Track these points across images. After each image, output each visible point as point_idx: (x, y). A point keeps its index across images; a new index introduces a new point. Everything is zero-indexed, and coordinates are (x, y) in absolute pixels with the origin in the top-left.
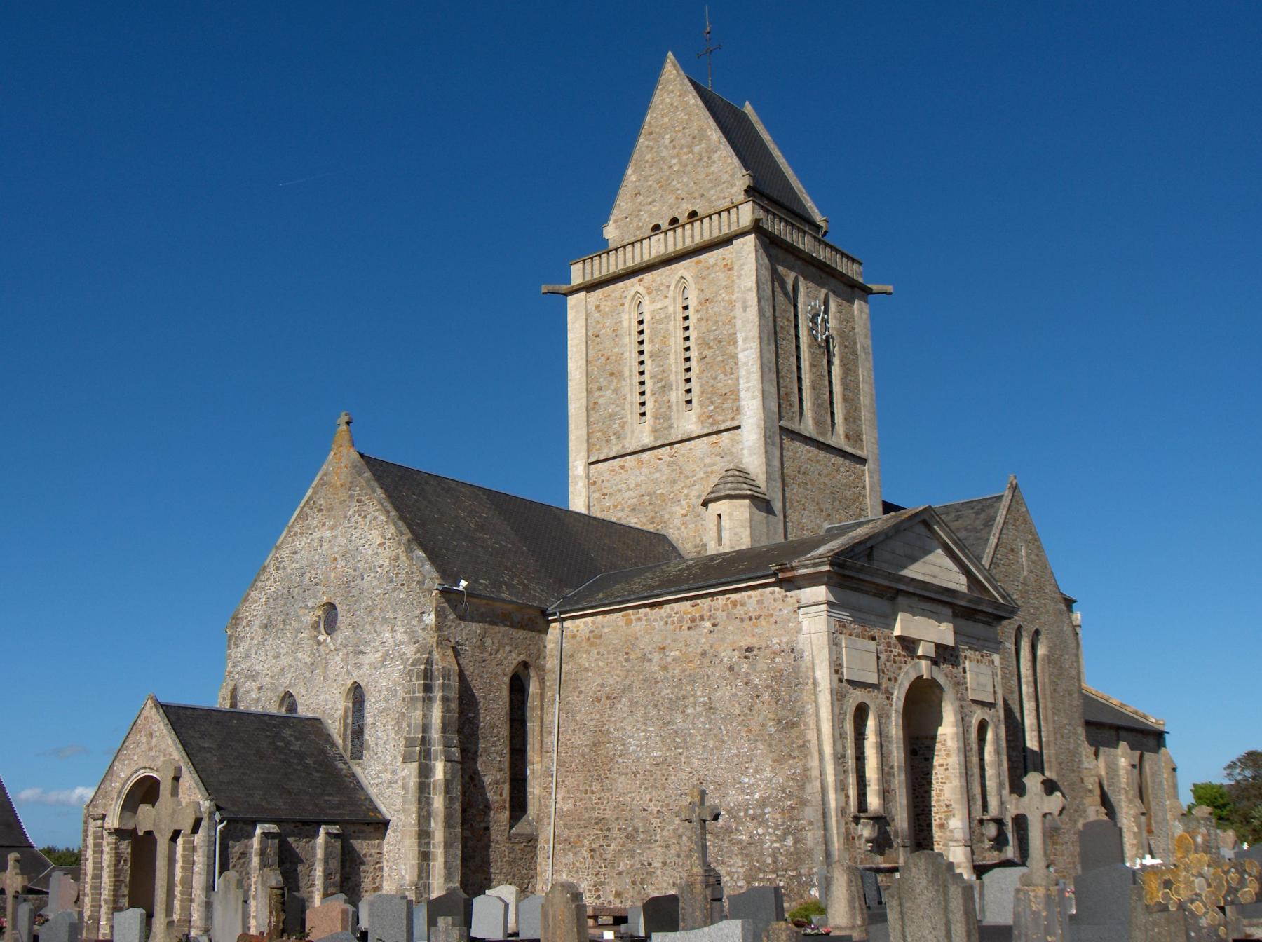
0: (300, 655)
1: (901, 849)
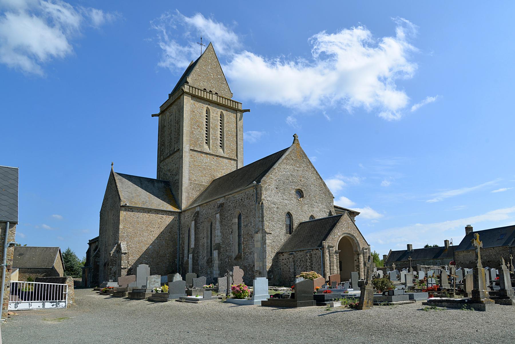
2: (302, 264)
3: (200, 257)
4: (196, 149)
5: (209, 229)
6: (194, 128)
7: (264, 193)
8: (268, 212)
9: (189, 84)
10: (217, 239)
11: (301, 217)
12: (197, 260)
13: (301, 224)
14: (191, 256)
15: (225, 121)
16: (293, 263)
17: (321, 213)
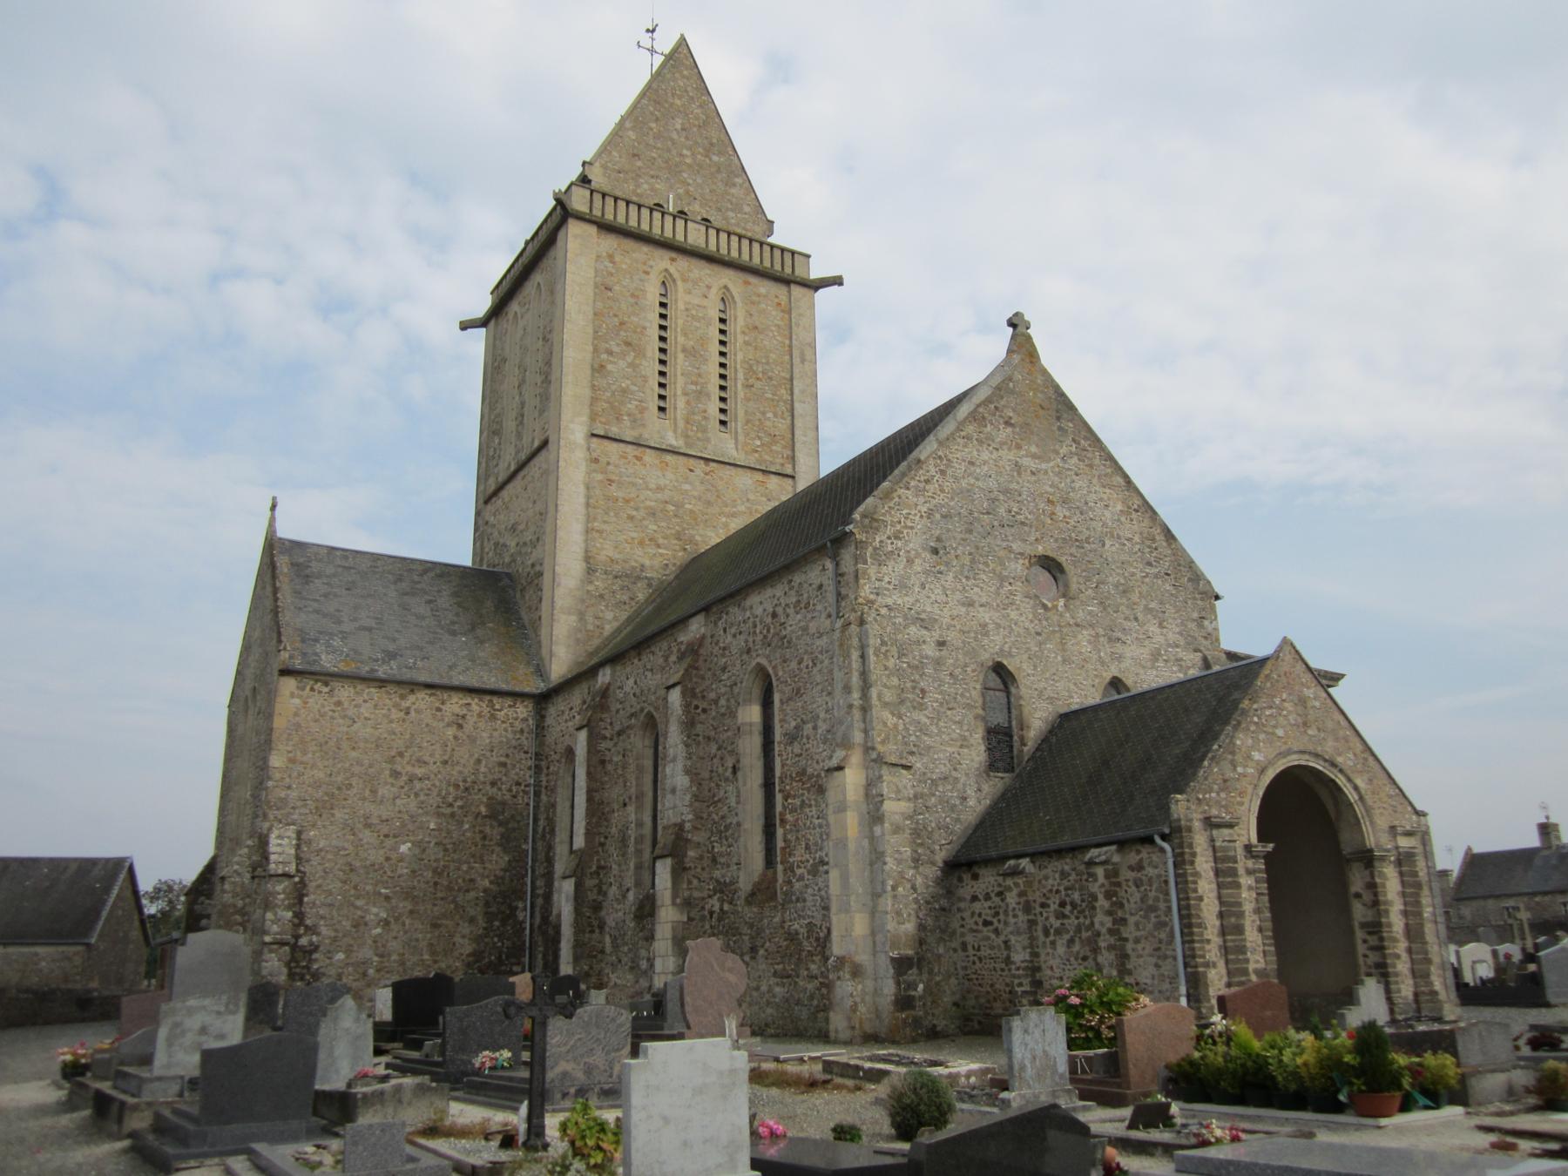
0: (1014, 615)
1: (863, 958)
2: (1072, 922)
3: (613, 891)
4: (614, 430)
5: (648, 763)
6: (610, 353)
7: (872, 571)
8: (891, 663)
9: (594, 185)
10: (677, 807)
11: (1058, 685)
12: (597, 907)
13: (1065, 717)
14: (568, 886)
15: (741, 322)
16: (1022, 917)
17: (1153, 662)
